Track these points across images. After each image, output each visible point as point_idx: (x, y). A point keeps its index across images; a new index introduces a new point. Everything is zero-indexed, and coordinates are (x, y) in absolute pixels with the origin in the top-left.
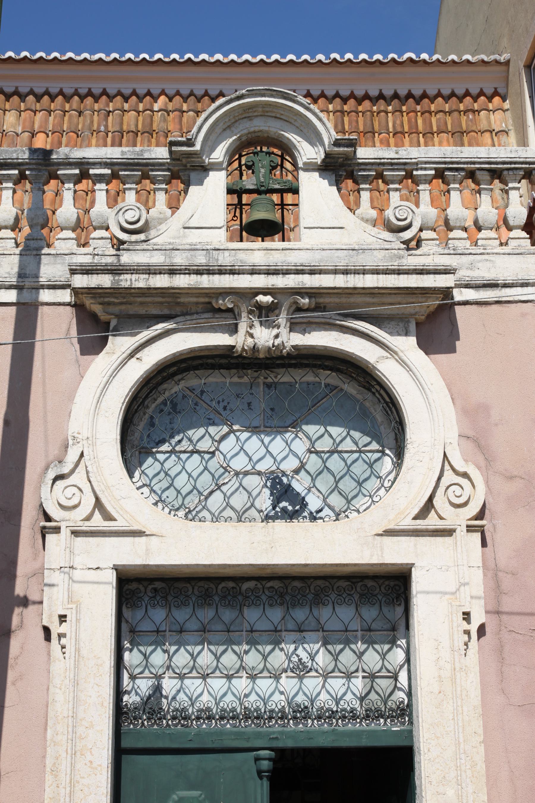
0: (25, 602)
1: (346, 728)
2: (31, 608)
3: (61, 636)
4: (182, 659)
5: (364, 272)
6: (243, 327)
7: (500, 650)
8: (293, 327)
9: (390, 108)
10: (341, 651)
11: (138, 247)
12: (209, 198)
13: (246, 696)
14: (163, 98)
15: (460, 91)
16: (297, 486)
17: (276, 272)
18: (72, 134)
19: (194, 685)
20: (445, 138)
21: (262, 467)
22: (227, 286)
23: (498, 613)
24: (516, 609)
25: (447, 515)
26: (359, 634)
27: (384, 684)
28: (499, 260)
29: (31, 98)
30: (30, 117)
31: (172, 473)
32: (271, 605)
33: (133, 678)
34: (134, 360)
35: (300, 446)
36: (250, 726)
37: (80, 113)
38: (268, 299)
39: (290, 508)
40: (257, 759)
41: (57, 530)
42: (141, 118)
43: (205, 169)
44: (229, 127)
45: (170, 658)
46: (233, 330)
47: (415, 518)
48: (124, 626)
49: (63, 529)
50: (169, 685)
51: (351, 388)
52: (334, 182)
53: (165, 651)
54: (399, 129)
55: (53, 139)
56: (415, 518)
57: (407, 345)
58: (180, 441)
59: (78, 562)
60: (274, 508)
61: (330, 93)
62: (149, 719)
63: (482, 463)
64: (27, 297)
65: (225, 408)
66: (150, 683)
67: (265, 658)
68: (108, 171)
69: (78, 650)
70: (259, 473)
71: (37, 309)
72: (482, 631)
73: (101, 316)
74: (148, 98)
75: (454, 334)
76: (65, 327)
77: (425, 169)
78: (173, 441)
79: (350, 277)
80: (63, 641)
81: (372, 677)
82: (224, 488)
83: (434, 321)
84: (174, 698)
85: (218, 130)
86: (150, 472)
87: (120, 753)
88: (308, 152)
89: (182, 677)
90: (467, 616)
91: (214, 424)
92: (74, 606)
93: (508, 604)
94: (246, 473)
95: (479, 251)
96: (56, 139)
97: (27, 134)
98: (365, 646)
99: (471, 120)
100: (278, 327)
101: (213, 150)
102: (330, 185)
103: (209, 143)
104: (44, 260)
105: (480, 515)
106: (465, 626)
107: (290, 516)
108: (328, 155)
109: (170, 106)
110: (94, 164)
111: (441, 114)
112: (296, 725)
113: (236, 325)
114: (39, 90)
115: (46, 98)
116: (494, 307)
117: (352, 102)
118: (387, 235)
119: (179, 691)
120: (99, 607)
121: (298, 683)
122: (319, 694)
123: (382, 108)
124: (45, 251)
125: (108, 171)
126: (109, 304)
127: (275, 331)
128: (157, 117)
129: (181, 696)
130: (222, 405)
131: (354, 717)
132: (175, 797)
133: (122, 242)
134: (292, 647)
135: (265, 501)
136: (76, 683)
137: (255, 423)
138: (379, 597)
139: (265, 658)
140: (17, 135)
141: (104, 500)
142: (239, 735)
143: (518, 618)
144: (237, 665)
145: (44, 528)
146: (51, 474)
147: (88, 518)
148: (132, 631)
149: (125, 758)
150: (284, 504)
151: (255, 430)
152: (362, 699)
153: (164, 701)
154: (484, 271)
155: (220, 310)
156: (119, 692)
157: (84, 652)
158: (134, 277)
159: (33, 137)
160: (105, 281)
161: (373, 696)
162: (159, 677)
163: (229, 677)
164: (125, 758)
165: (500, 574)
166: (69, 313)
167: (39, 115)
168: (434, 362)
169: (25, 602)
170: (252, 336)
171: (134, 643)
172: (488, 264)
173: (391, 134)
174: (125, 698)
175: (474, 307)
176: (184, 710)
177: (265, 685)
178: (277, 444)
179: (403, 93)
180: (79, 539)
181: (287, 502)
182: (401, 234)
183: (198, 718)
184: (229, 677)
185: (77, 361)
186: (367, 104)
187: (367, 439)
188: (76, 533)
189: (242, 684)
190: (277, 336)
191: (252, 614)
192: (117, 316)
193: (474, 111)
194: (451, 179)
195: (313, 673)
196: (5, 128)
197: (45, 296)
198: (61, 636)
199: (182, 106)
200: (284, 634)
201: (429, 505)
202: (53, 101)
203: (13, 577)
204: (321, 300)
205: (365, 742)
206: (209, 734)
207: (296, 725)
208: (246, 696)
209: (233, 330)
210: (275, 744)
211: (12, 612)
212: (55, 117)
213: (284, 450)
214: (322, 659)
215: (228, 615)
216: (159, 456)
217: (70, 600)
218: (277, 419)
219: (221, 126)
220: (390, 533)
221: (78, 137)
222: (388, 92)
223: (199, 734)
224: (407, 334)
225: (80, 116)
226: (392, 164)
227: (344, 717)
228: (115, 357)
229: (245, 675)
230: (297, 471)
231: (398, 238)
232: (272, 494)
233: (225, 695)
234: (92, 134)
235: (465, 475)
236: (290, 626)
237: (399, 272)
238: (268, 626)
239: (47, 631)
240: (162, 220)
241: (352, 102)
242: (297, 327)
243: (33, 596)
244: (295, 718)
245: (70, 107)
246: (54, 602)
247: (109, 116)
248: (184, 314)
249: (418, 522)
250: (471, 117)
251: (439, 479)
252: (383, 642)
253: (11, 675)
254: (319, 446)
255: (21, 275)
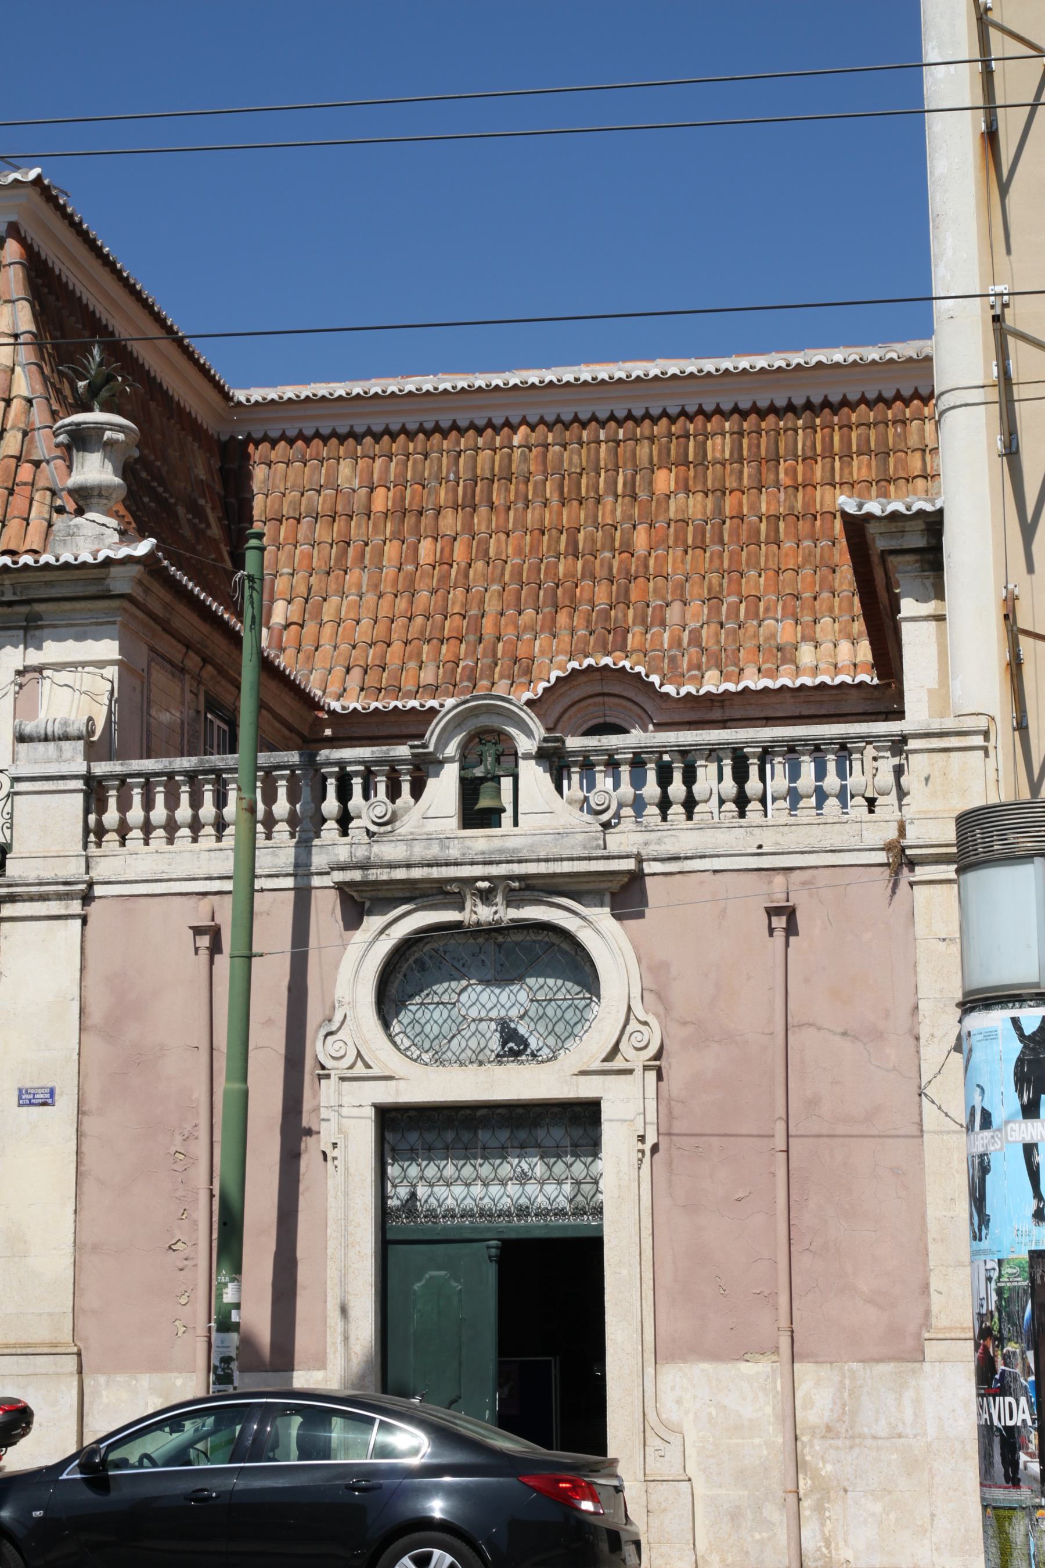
0: (309, 1132)
1: (557, 1223)
2: (314, 1137)
3: (335, 1159)
4: (431, 1171)
5: (562, 860)
6: (468, 904)
7: (670, 1163)
8: (509, 904)
9: (800, 422)
10: (555, 1163)
11: (385, 839)
12: (444, 788)
13: (481, 1199)
14: (523, 429)
15: (889, 394)
16: (522, 1030)
17: (491, 863)
18: (416, 486)
19: (440, 1191)
20: (865, 463)
21: (493, 1014)
22: (452, 876)
23: (670, 1134)
24: (684, 1131)
25: (632, 1057)
26: (569, 1149)
27: (586, 1188)
28: (682, 835)
29: (368, 440)
30: (368, 467)
31: (423, 1021)
32: (499, 1128)
33: (394, 1186)
34: (383, 936)
35: (523, 996)
36: (484, 1222)
37: (426, 456)
38: (485, 885)
39: (515, 1048)
40: (488, 1247)
41: (328, 1076)
42: (497, 457)
43: (441, 763)
44: (459, 725)
45: (422, 1171)
46: (461, 908)
47: (604, 1061)
48: (387, 1147)
49: (332, 1076)
50: (422, 1191)
51: (565, 946)
52: (548, 769)
53: (419, 1165)
54: (809, 454)
55: (395, 493)
56: (604, 1061)
57: (602, 915)
58: (428, 995)
59: (346, 1100)
60: (503, 1048)
61: (727, 406)
62: (407, 1217)
63: (661, 1011)
64: (302, 883)
65: (463, 965)
66: (408, 1189)
67: (495, 1170)
68: (362, 768)
69: (347, 1169)
70: (491, 1020)
71: (310, 893)
72: (655, 1149)
73: (359, 901)
74: (506, 429)
75: (643, 901)
76: (330, 906)
77: (625, 753)
78: (423, 994)
79: (551, 864)
80: (336, 1162)
81: (578, 1183)
82: (463, 1033)
83: (625, 894)
84: (426, 1201)
85: (450, 729)
86: (406, 1021)
87: (386, 1244)
88: (525, 745)
89: (431, 1185)
90: (642, 1139)
91: (454, 979)
92: (342, 1136)
93: (678, 1127)
94: (481, 1020)
95: (666, 828)
96: (398, 494)
97: (364, 490)
98: (573, 1159)
99: (899, 435)
100: (497, 905)
101: (446, 746)
102: (545, 771)
103: (443, 741)
104: (314, 850)
105: (658, 1056)
106: (640, 1146)
107: (515, 1054)
108: (539, 748)
109: (533, 438)
110: (350, 763)
111: (863, 427)
112: (519, 1221)
113: (464, 904)
114: (378, 428)
115: (386, 438)
116: (677, 876)
117: (753, 417)
118: (589, 818)
119: (429, 1196)
120: (362, 1137)
121: (516, 1189)
122: (537, 1197)
123: (790, 425)
124: (316, 842)
125: (362, 768)
126: (362, 891)
127: (494, 909)
128: (517, 453)
129: (432, 1200)
130: (461, 962)
131: (566, 1214)
132: (427, 1276)
133: (374, 834)
134: (516, 1161)
135: (495, 1044)
136: (346, 1194)
137: (489, 977)
138: (574, 1124)
139: (495, 1170)
140: (354, 491)
141: (362, 1053)
142: (474, 1229)
143: (685, 1138)
144: (474, 1176)
145: (319, 1075)
146: (323, 1032)
147: (351, 1067)
148: (393, 1150)
149: (391, 1247)
150: (511, 1045)
151: (487, 982)
152: (571, 1201)
153: (418, 1203)
154: (670, 847)
155: (448, 893)
156: (382, 1197)
157: (352, 1170)
158: (379, 871)
159: (372, 492)
160: (356, 875)
161: (579, 1198)
162: (415, 1186)
163: (468, 1185)
164: (391, 1248)
165: (673, 1103)
166: (334, 894)
167: (379, 462)
168: (625, 929)
169: (309, 1132)
170: (476, 913)
171: (394, 1160)
172: (673, 839)
173: (800, 459)
174: (389, 1202)
175: (661, 877)
176: (435, 1210)
177: (495, 1190)
178: (504, 995)
179: (817, 400)
180: (345, 1083)
181: (513, 1046)
182: (600, 817)
183: (444, 1217)
184: (468, 1185)
185: (341, 936)
186: (771, 418)
187: (577, 989)
188: (343, 1079)
189: (477, 1190)
190: (496, 913)
191: (483, 1135)
192: (369, 899)
193: (904, 422)
194: (647, 760)
195: (533, 1181)
196: (339, 482)
197: (316, 881)
198: (335, 1159)
199: (547, 437)
200: (510, 1150)
201: (615, 1050)
202: (394, 441)
203: (300, 1112)
204: (529, 882)
205: (570, 1234)
206: (453, 1228)
207: (519, 1221)
208: (481, 1199)
209: (461, 908)
210: (502, 1236)
211: (300, 1140)
212: (397, 464)
213: (511, 1000)
214: (540, 1169)
215: (466, 1136)
216: (410, 1007)
217: (340, 1131)
218: (503, 975)
219: (452, 725)
220: (583, 1073)
221: (424, 488)
222: (799, 401)
223: (445, 1229)
224: (602, 905)
225: (426, 459)
226: (596, 751)
227: (555, 1215)
228: (369, 934)
229: (480, 1183)
230: (522, 1017)
231: (597, 820)
232: (502, 1037)
233: (465, 1198)
234: (441, 484)
235: (646, 1023)
236: (515, 1144)
237: (590, 859)
238: (497, 1144)
239: (324, 1154)
240: (407, 810)
241: (753, 417)
242: (513, 904)
243: (315, 1128)
244: (517, 1215)
245: (415, 448)
246: (327, 1134)
247: (460, 456)
248: (422, 896)
249: (605, 1064)
250: (899, 430)
251: (624, 1027)
252: (587, 1156)
253: (302, 1187)
254: (540, 996)
255: (296, 865)
